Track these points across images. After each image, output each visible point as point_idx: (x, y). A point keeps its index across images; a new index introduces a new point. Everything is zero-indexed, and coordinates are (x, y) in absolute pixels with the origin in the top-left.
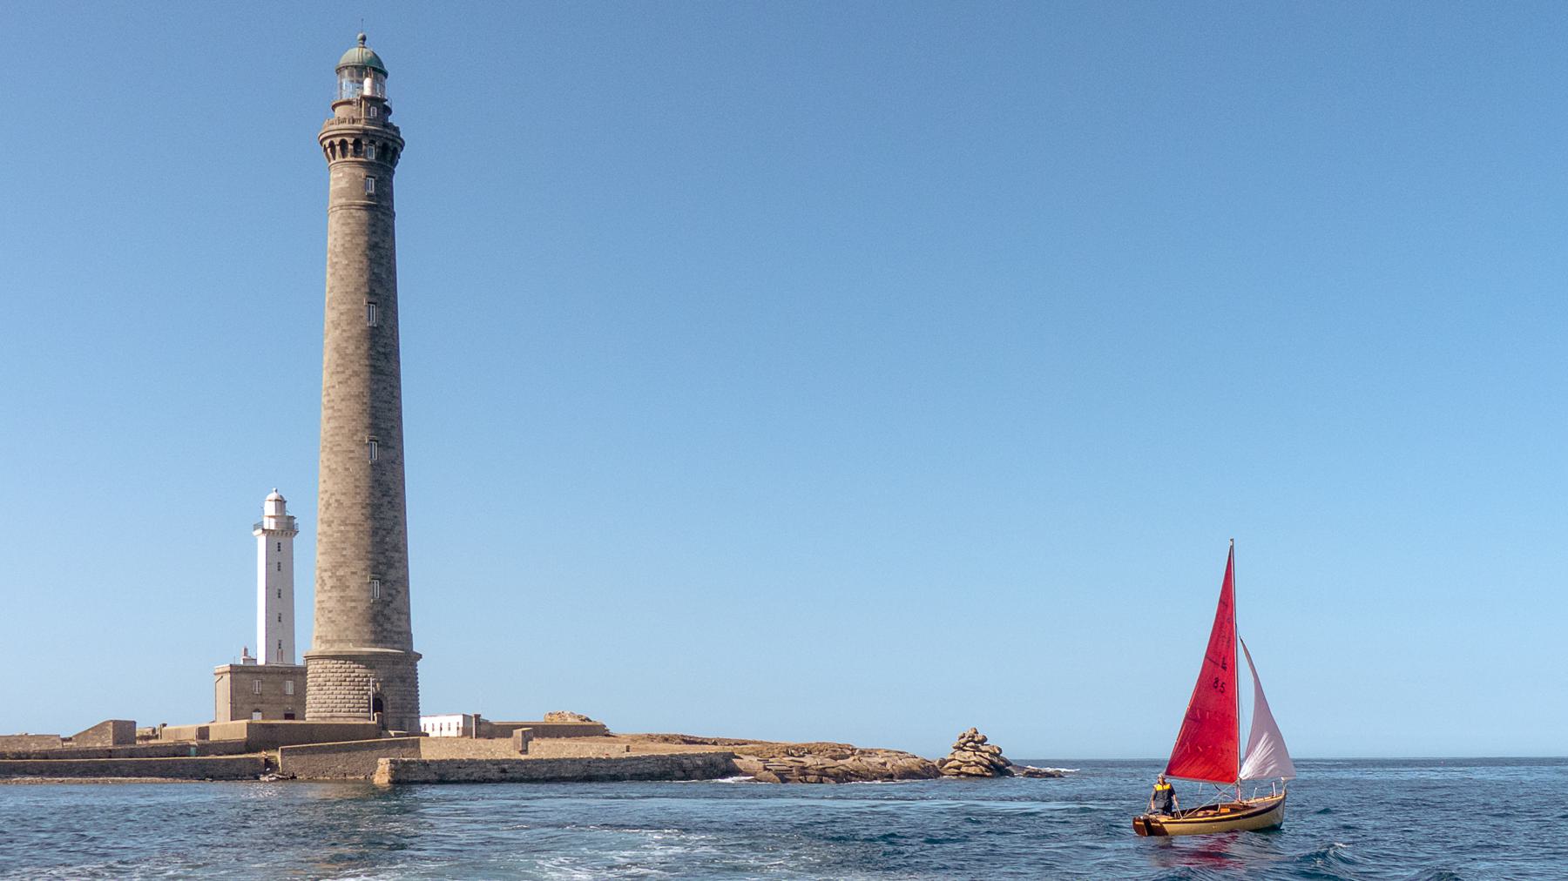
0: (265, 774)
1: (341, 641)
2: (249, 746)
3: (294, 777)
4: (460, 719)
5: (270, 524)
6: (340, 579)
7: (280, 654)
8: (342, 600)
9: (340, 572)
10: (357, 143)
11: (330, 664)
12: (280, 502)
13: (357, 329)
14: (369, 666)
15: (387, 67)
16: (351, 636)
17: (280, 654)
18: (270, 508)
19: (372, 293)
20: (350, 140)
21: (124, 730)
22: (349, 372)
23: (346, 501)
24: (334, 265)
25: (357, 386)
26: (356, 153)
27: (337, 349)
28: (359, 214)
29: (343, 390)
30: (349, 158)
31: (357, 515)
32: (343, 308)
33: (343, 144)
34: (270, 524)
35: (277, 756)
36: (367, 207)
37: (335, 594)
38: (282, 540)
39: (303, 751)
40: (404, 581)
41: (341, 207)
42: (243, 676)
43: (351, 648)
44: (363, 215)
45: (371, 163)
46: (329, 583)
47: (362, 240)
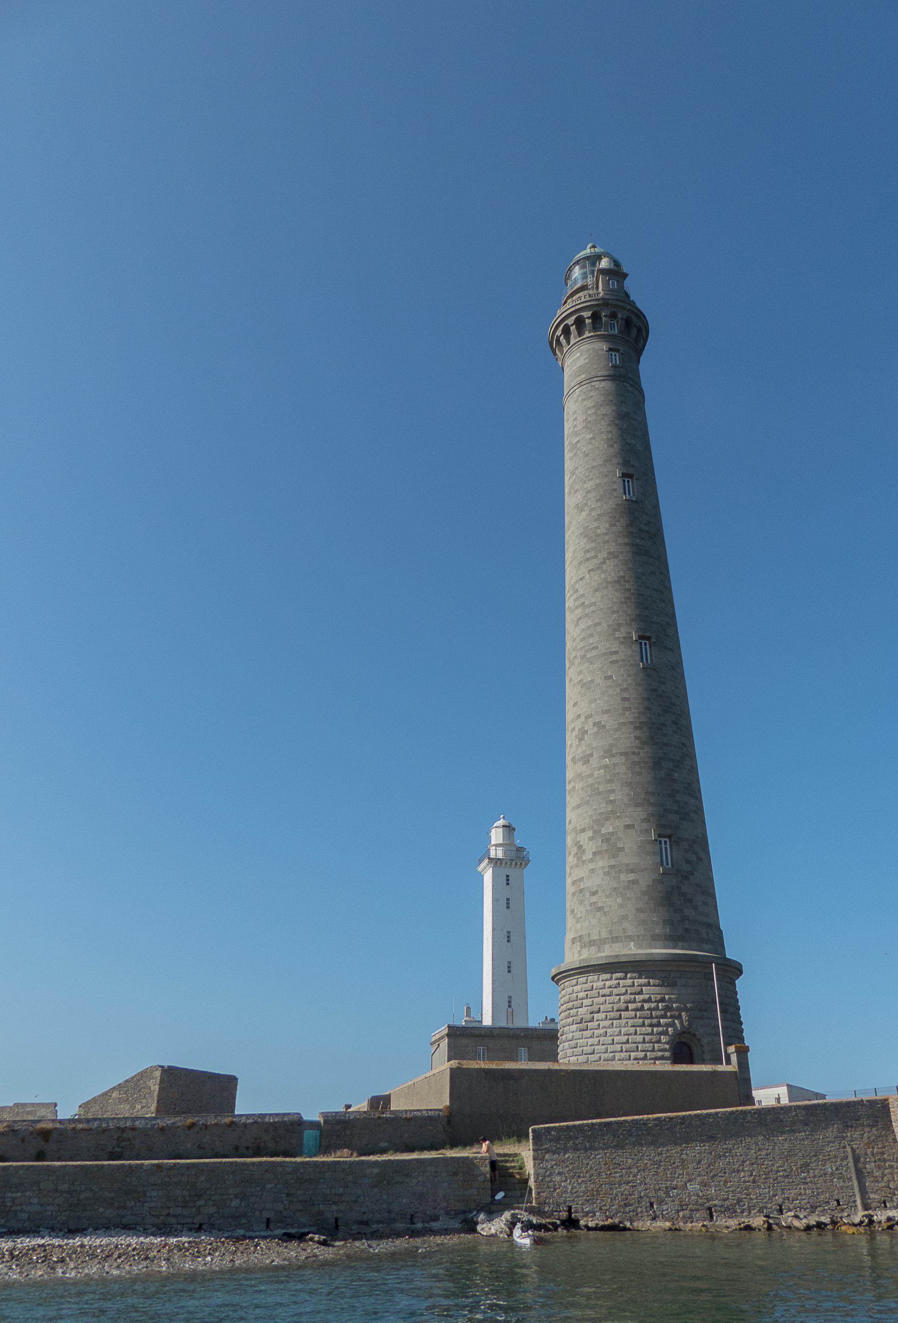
0: (492, 1210)
1: (615, 940)
2: (454, 1127)
3: (571, 1223)
4: (785, 1088)
5: (497, 853)
6: (607, 839)
7: (511, 1015)
8: (613, 871)
9: (607, 829)
10: (595, 317)
11: (598, 981)
12: (509, 829)
13: (611, 504)
14: (667, 982)
15: (625, 270)
16: (631, 928)
17: (511, 1015)
18: (496, 836)
19: (625, 463)
20: (587, 314)
21: (195, 1093)
22: (603, 554)
23: (610, 722)
24: (574, 446)
25: (613, 570)
26: (594, 328)
27: (585, 534)
28: (603, 384)
29: (597, 578)
30: (587, 334)
31: (627, 739)
32: (589, 485)
33: (580, 322)
34: (497, 853)
35: (525, 1155)
36: (612, 378)
37: (601, 863)
38: (512, 872)
39: (589, 1140)
40: (702, 842)
41: (580, 384)
42: (464, 1041)
43: (632, 950)
44: (607, 385)
45: (614, 336)
46: (590, 849)
47: (608, 410)
